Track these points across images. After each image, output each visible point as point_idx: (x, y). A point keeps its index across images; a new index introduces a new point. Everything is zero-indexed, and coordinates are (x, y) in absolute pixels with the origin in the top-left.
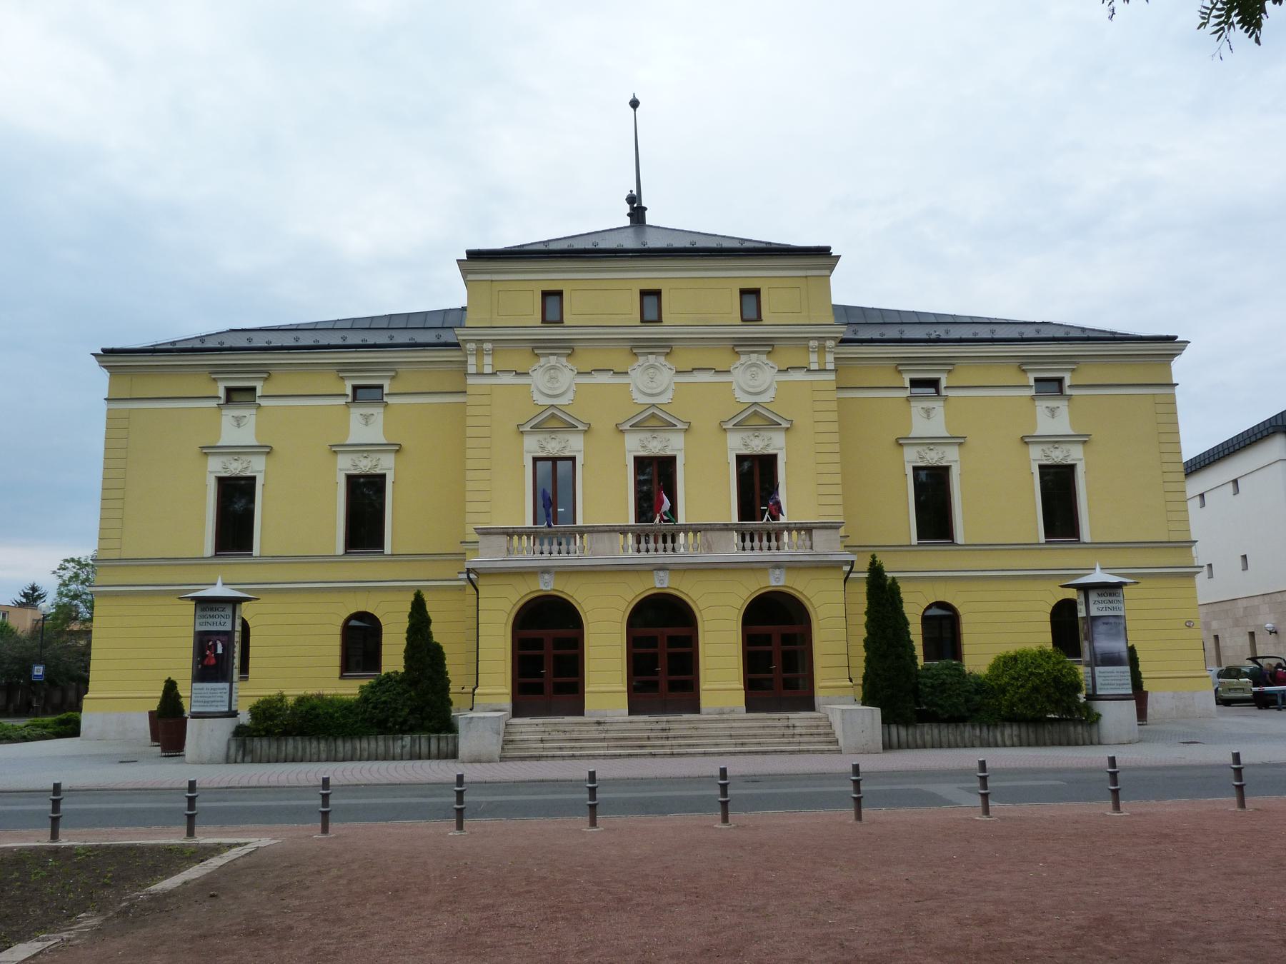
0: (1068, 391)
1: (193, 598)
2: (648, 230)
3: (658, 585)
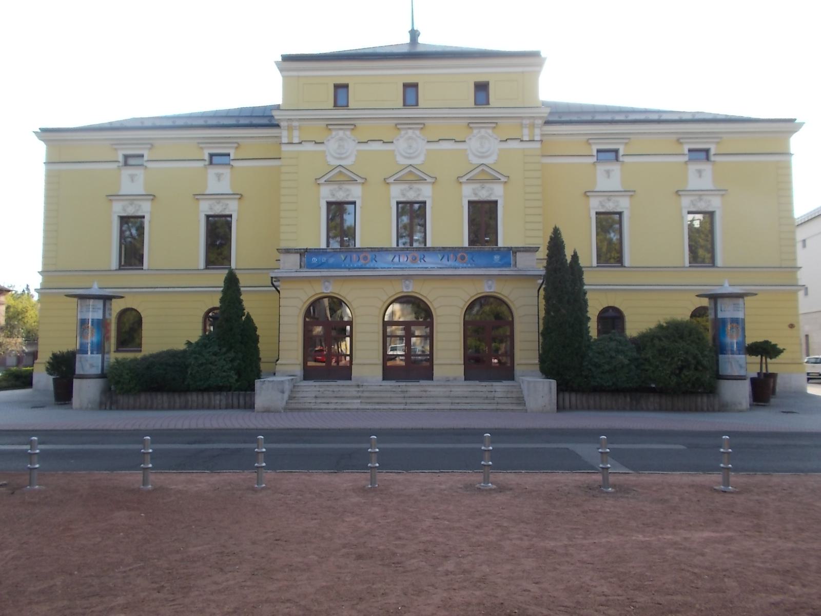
0: (712, 158)
3: (405, 290)
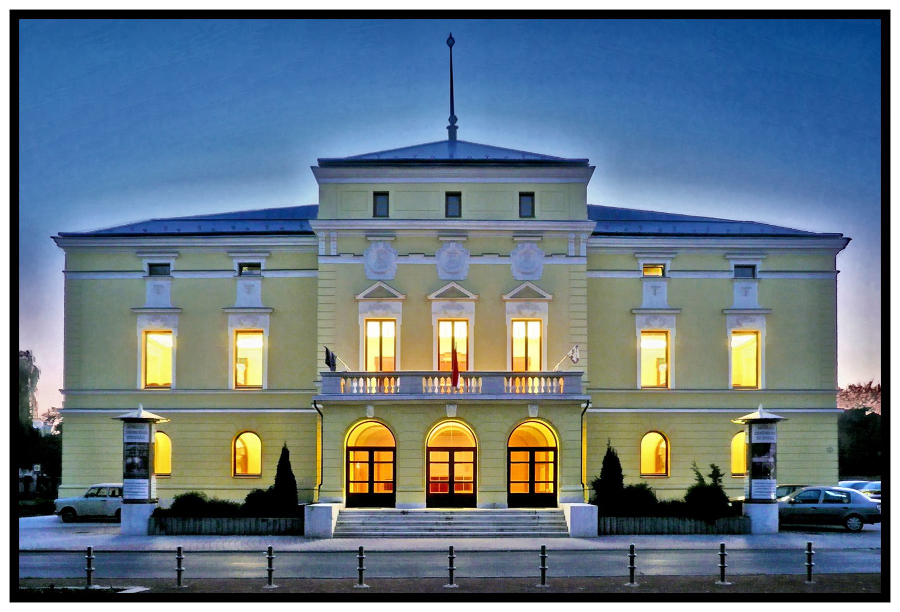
0: (758, 276)
1: (122, 419)
2: (458, 144)
